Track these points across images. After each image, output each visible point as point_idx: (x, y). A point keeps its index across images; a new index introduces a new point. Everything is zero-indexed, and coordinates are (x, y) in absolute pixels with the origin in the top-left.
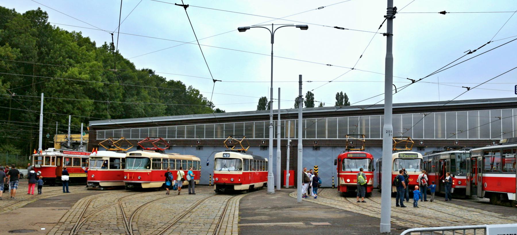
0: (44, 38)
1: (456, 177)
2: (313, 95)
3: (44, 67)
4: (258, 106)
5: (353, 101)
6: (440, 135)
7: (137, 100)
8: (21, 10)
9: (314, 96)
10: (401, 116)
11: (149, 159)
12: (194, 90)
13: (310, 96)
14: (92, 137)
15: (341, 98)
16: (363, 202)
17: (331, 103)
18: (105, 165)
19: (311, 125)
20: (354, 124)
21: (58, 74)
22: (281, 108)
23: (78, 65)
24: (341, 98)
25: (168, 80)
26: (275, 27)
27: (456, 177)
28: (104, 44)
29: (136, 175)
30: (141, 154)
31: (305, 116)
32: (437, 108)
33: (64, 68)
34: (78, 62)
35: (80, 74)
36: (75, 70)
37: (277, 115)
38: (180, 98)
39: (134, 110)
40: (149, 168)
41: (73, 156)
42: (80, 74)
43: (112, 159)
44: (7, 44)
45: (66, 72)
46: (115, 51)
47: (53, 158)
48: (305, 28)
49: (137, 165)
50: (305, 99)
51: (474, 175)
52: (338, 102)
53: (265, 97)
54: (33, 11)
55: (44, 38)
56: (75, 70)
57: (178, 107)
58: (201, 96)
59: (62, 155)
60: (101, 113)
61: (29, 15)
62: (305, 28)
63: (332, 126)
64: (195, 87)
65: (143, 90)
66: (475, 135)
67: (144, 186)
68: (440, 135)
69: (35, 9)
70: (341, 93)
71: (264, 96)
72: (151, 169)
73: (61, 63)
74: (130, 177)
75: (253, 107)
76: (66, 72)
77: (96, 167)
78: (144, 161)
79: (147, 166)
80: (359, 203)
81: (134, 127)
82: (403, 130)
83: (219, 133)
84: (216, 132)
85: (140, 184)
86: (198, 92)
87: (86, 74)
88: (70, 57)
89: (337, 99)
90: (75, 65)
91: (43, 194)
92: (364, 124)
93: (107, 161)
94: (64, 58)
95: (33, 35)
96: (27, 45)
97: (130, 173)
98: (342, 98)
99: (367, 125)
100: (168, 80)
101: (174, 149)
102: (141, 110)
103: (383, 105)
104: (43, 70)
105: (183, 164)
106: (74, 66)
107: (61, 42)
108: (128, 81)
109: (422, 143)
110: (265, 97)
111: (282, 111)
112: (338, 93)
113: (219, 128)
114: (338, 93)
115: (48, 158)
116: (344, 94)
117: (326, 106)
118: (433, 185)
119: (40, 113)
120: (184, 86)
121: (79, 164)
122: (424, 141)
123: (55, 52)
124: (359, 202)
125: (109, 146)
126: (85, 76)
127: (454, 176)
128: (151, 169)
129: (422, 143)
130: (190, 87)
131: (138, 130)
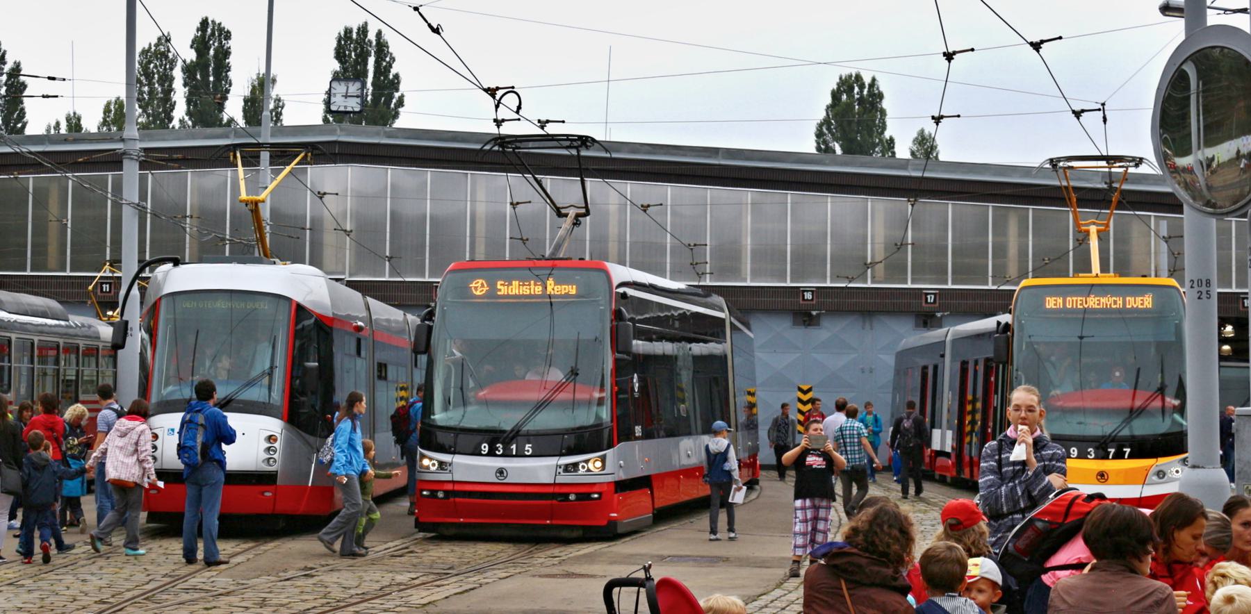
2: (228, 36)
9: (232, 44)
13: (212, 42)
31: (153, 160)
59: (1209, 152)
89: (340, 55)
116: (372, 36)
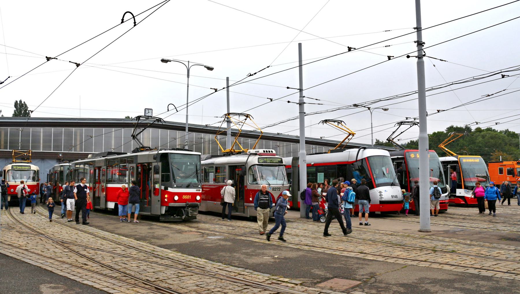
1: (170, 190)
5: (38, 113)
6: (78, 149)
16: (366, 224)
20: (69, 135)
22: (189, 122)
27: (170, 190)
32: (26, 124)
51: (97, 185)
52: (17, 110)
63: (47, 137)
66: (39, 148)
68: (78, 149)
80: (361, 226)
82: (115, 146)
83: (78, 147)
92: (78, 138)
99: (6, 135)
109: (61, 155)
111: (189, 124)
112: (17, 101)
114: (17, 101)
116: (23, 103)
117: (32, 115)
118: (34, 196)
122: (63, 154)
124: (361, 224)
127: (166, 188)
129: (61, 155)
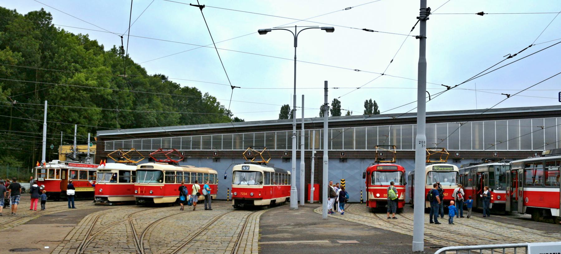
0: (48, 42)
1: (495, 191)
2: (340, 102)
3: (47, 72)
4: (280, 115)
5: (383, 109)
6: (477, 146)
7: (149, 108)
8: (23, 11)
9: (341, 104)
10: (436, 125)
11: (161, 172)
12: (210, 97)
13: (336, 103)
14: (100, 148)
15: (370, 106)
16: (394, 218)
17: (359, 111)
18: (114, 179)
19: (338, 135)
20: (384, 135)
21: (63, 80)
22: (305, 117)
23: (85, 70)
24: (370, 106)
25: (182, 86)
26: (298, 30)
27: (495, 191)
28: (113, 47)
29: (147, 189)
30: (153, 167)
32: (474, 117)
33: (69, 74)
34: (84, 67)
35: (87, 80)
36: (81, 76)
37: (301, 124)
38: (196, 106)
39: (145, 119)
40: (162, 182)
41: (79, 169)
42: (87, 80)
43: (122, 172)
44: (8, 48)
45: (72, 78)
46: (125, 55)
47: (58, 171)
48: (331, 30)
49: (149, 178)
50: (331, 107)
51: (514, 189)
52: (367, 110)
53: (288, 105)
54: (36, 12)
55: (48, 42)
56: (81, 76)
57: (193, 116)
58: (218, 103)
59: (67, 167)
60: (109, 123)
61: (32, 16)
62: (331, 30)
63: (360, 136)
64: (212, 94)
65: (155, 98)
66: (516, 146)
67: (156, 201)
68: (477, 146)
69: (38, 9)
70: (371, 101)
71: (286, 104)
72: (164, 183)
73: (66, 68)
74: (142, 192)
75: (274, 116)
76: (72, 78)
77: (104, 181)
78: (157, 174)
79: (160, 179)
80: (389, 220)
81: (145, 137)
82: (437, 141)
83: (238, 144)
84: (235, 142)
85: (152, 199)
86: (214, 99)
87: (94, 80)
88: (76, 62)
89: (365, 107)
90: (82, 70)
91: (46, 210)
92: (395, 134)
93: (116, 174)
94: (69, 63)
95: (36, 38)
96: (29, 49)
97: (141, 187)
98: (371, 106)
99: (398, 135)
100: (182, 86)
101: (189, 161)
102: (153, 119)
103: (415, 114)
104: (47, 75)
105: (198, 178)
106: (80, 72)
107: (66, 45)
108: (139, 88)
109: (457, 154)
110: (288, 105)
111: (306, 120)
112: (367, 101)
113: (238, 138)
114: (367, 101)
115: (52, 170)
116: (373, 102)
117: (353, 114)
118: (470, 200)
119: (43, 122)
120: (200, 93)
121: (85, 177)
122: (460, 152)
123: (60, 56)
124: (389, 218)
125: (118, 158)
126: (92, 82)
127: (492, 190)
128: (164, 183)
129: (457, 154)
130: (206, 94)
131: (150, 140)
